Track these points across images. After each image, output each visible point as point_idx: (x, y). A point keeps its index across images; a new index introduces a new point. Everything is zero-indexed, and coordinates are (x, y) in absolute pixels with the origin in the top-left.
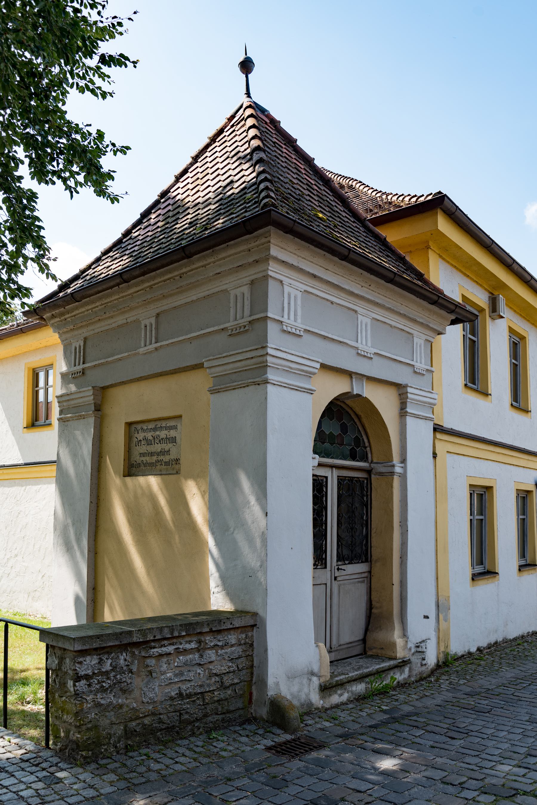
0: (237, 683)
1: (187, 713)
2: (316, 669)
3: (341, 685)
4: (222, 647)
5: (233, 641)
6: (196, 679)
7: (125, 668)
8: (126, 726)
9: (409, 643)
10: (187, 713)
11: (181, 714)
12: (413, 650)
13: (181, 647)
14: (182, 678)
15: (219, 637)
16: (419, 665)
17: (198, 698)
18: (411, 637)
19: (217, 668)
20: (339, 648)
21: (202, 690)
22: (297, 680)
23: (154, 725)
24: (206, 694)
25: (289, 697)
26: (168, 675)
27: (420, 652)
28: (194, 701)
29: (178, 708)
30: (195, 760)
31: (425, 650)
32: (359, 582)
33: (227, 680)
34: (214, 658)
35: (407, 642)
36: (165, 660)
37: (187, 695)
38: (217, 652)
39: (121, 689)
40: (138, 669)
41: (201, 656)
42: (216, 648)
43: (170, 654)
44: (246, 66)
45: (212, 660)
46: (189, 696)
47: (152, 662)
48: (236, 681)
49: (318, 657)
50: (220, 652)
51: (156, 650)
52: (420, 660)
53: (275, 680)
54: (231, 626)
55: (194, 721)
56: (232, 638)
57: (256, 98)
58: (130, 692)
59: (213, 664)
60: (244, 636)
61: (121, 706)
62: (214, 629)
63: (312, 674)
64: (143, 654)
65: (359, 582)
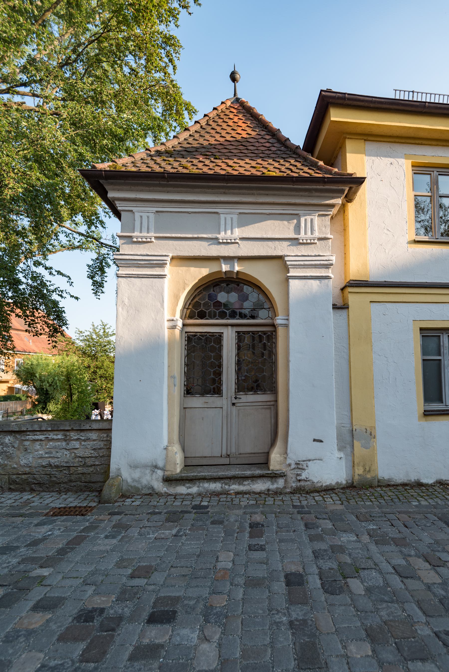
0: (98, 465)
1: (55, 477)
2: (161, 464)
3: (192, 480)
4: (84, 441)
5: (94, 438)
6: (63, 456)
7: (9, 444)
8: (9, 478)
9: (288, 459)
10: (55, 477)
11: (51, 477)
12: (293, 466)
13: (50, 437)
14: (52, 456)
15: (82, 434)
16: (294, 479)
17: (65, 470)
18: (290, 455)
19: (80, 453)
20: (239, 456)
21: (68, 465)
22: (139, 470)
23: (30, 480)
24: (71, 468)
25: (129, 480)
26: (40, 452)
27: (300, 469)
28: (61, 471)
29: (48, 473)
30: (155, 506)
31: (306, 468)
32: (263, 408)
33: (89, 462)
34: (78, 446)
35: (286, 458)
36: (38, 443)
37: (55, 466)
38: (81, 443)
39: (7, 456)
40: (18, 446)
41: (68, 444)
42: (80, 440)
43: (41, 440)
44: (233, 77)
45: (76, 447)
46: (57, 467)
47: (27, 443)
48: (97, 463)
49: (164, 456)
50: (83, 443)
51: (30, 437)
52: (295, 475)
53: (117, 467)
54: (90, 428)
55: (60, 483)
56: (94, 435)
57: (239, 96)
58: (12, 458)
59: (78, 450)
60: (105, 435)
61: (6, 465)
62: (75, 429)
63: (156, 467)
64: (23, 438)
65: (263, 408)
